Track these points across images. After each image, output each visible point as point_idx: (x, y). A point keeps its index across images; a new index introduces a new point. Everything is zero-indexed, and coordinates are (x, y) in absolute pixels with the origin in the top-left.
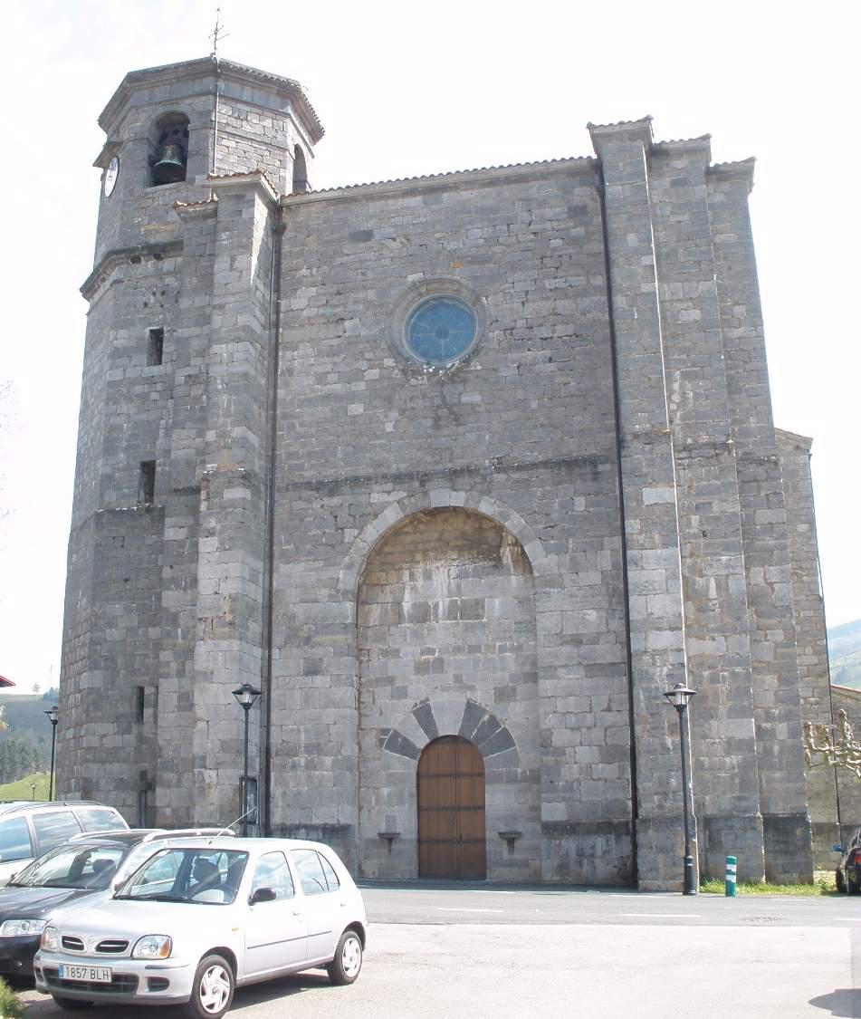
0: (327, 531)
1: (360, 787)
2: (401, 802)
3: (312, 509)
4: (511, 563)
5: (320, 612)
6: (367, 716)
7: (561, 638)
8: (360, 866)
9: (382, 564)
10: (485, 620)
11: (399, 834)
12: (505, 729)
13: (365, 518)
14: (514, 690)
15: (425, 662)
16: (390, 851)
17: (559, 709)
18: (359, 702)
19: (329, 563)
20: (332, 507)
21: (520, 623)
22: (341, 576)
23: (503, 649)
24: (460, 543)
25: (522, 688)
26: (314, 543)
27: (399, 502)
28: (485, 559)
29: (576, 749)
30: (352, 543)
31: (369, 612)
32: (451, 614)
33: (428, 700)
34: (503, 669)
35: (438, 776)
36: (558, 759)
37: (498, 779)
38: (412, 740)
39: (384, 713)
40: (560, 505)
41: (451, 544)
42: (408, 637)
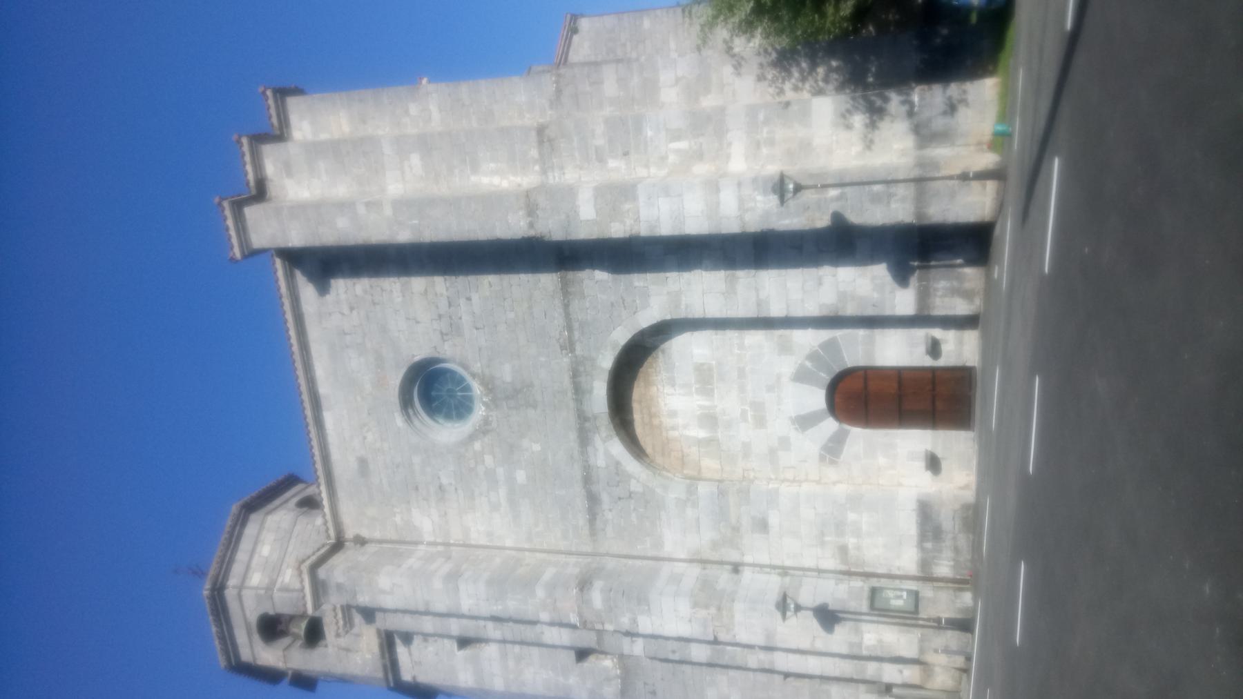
10: (714, 362)
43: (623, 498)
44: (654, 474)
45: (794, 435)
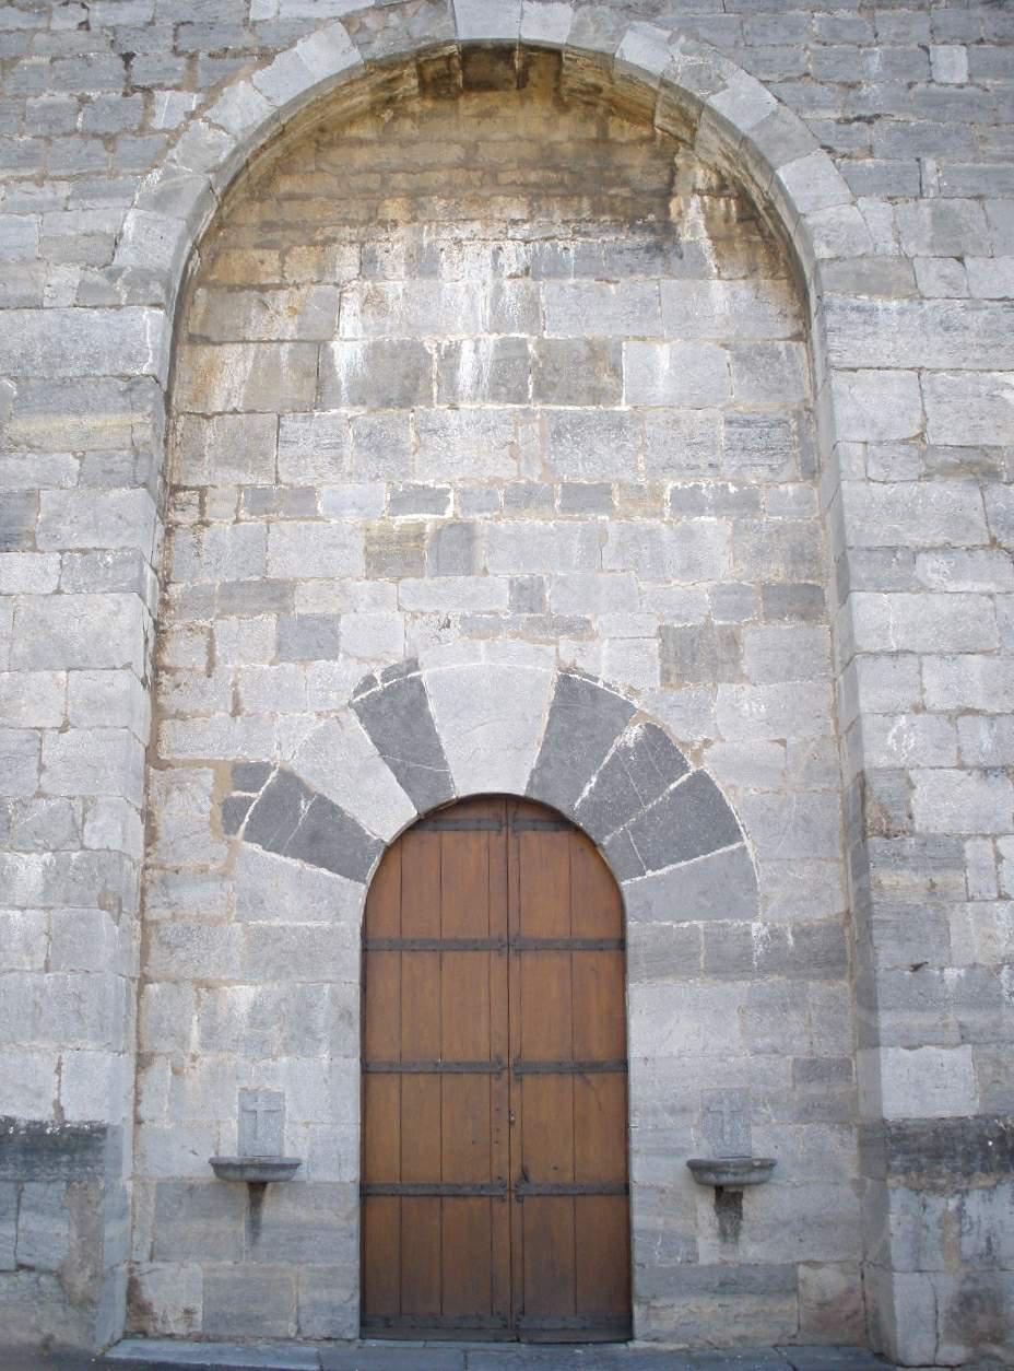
0: (94, 95)
1: (144, 980)
2: (302, 1037)
3: (48, 30)
4: (706, 244)
5: (44, 338)
6: (180, 716)
7: (923, 455)
8: (133, 1286)
9: (268, 226)
10: (623, 407)
11: (294, 1166)
12: (701, 779)
13: (228, 62)
14: (732, 641)
15: (403, 538)
16: (255, 1226)
17: (934, 699)
18: (158, 668)
19: (87, 185)
20: (114, 30)
21: (748, 423)
22: (129, 227)
23: (688, 503)
24: (533, 177)
25: (761, 638)
26: (39, 130)
27: (346, 21)
28: (618, 226)
29: (999, 842)
30: (175, 134)
31: (212, 368)
32: (506, 381)
33: (413, 664)
34: (691, 568)
35: (439, 947)
36: (938, 879)
37: (676, 960)
38: (347, 805)
39: (247, 707)
40: (888, 62)
41: (504, 178)
42: (349, 450)
43: (127, 66)
44: (216, 170)
45: (342, 675)
